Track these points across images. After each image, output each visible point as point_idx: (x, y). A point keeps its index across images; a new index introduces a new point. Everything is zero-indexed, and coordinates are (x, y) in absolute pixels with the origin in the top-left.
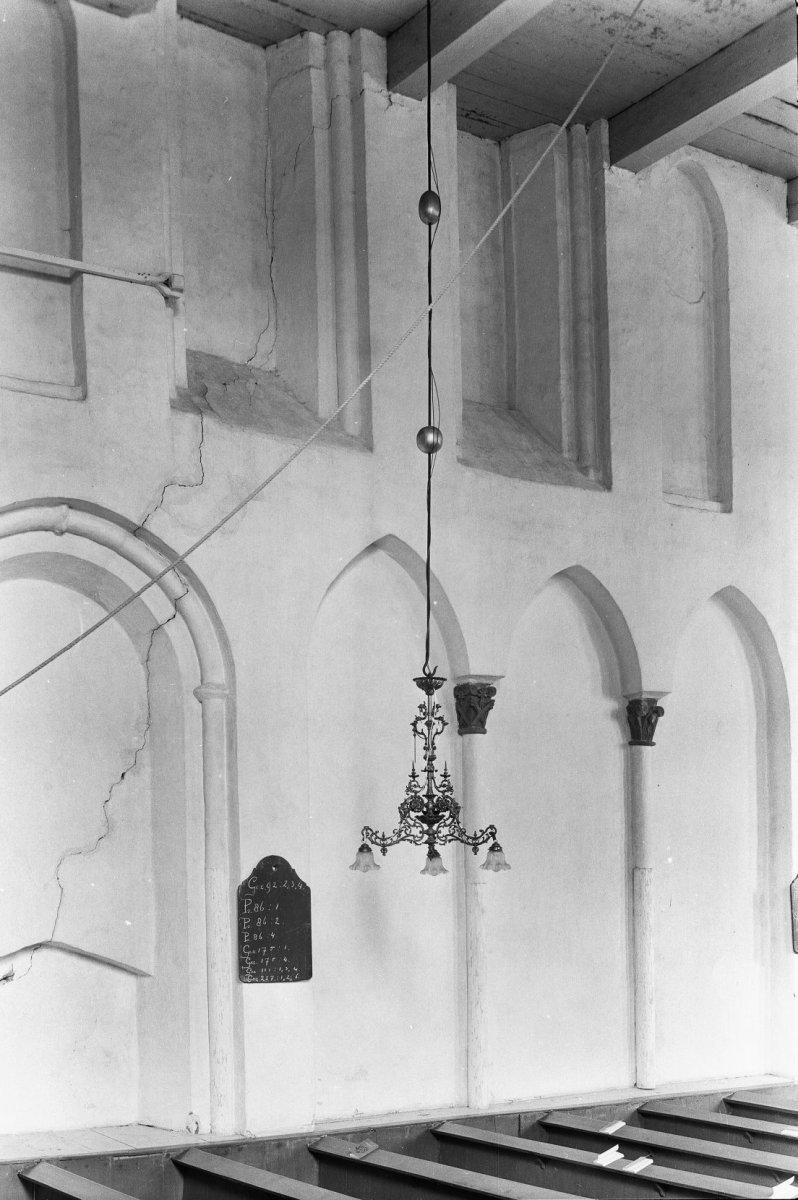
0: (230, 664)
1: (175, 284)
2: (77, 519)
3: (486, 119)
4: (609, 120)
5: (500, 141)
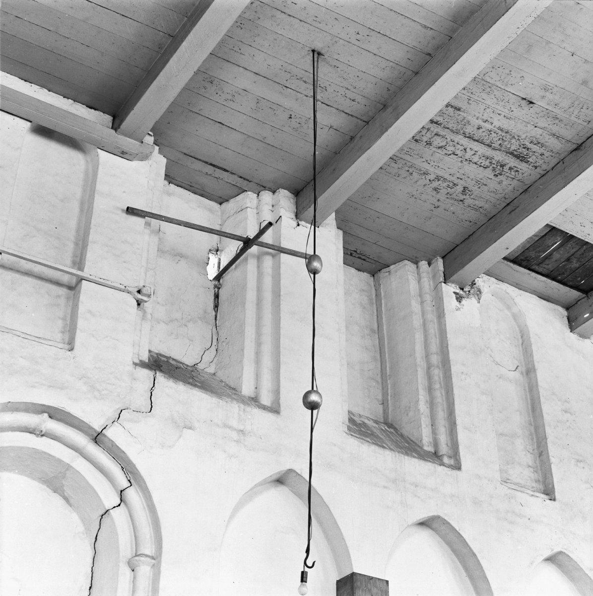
1: (144, 291)
3: (363, 257)
4: (443, 258)
5: (373, 274)
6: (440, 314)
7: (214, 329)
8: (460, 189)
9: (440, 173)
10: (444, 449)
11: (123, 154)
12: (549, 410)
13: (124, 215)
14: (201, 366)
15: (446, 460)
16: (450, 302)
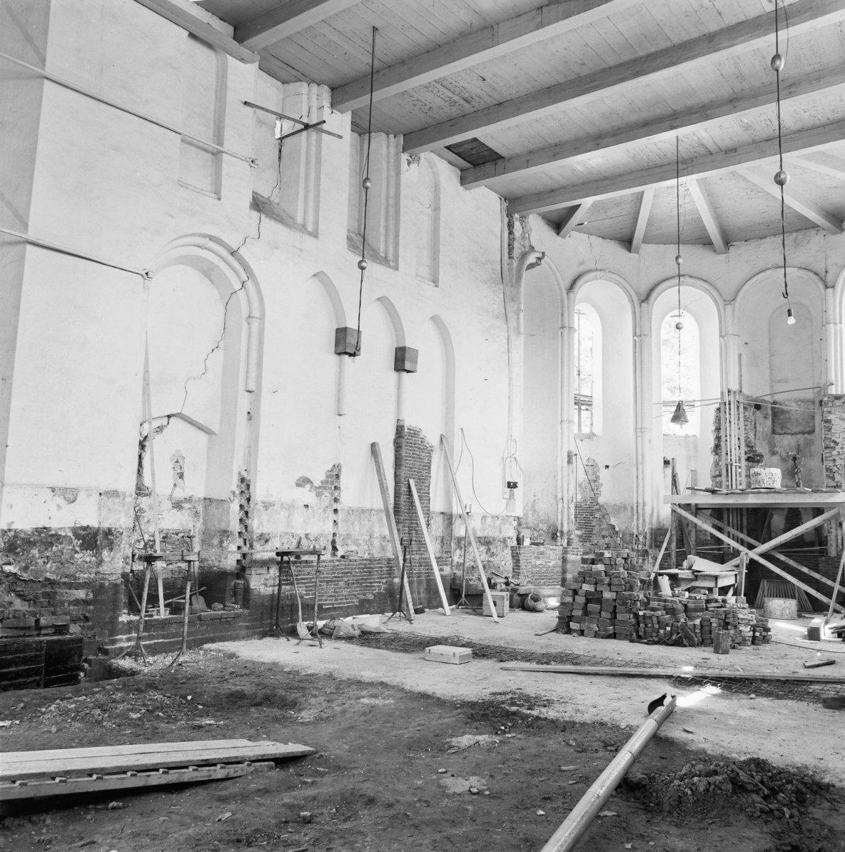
0: (261, 300)
1: (256, 162)
2: (211, 245)
6: (398, 173)
7: (279, 176)
8: (428, 107)
9: (420, 98)
10: (390, 257)
11: (242, 60)
12: (443, 233)
13: (243, 106)
14: (272, 199)
15: (391, 263)
16: (404, 165)
